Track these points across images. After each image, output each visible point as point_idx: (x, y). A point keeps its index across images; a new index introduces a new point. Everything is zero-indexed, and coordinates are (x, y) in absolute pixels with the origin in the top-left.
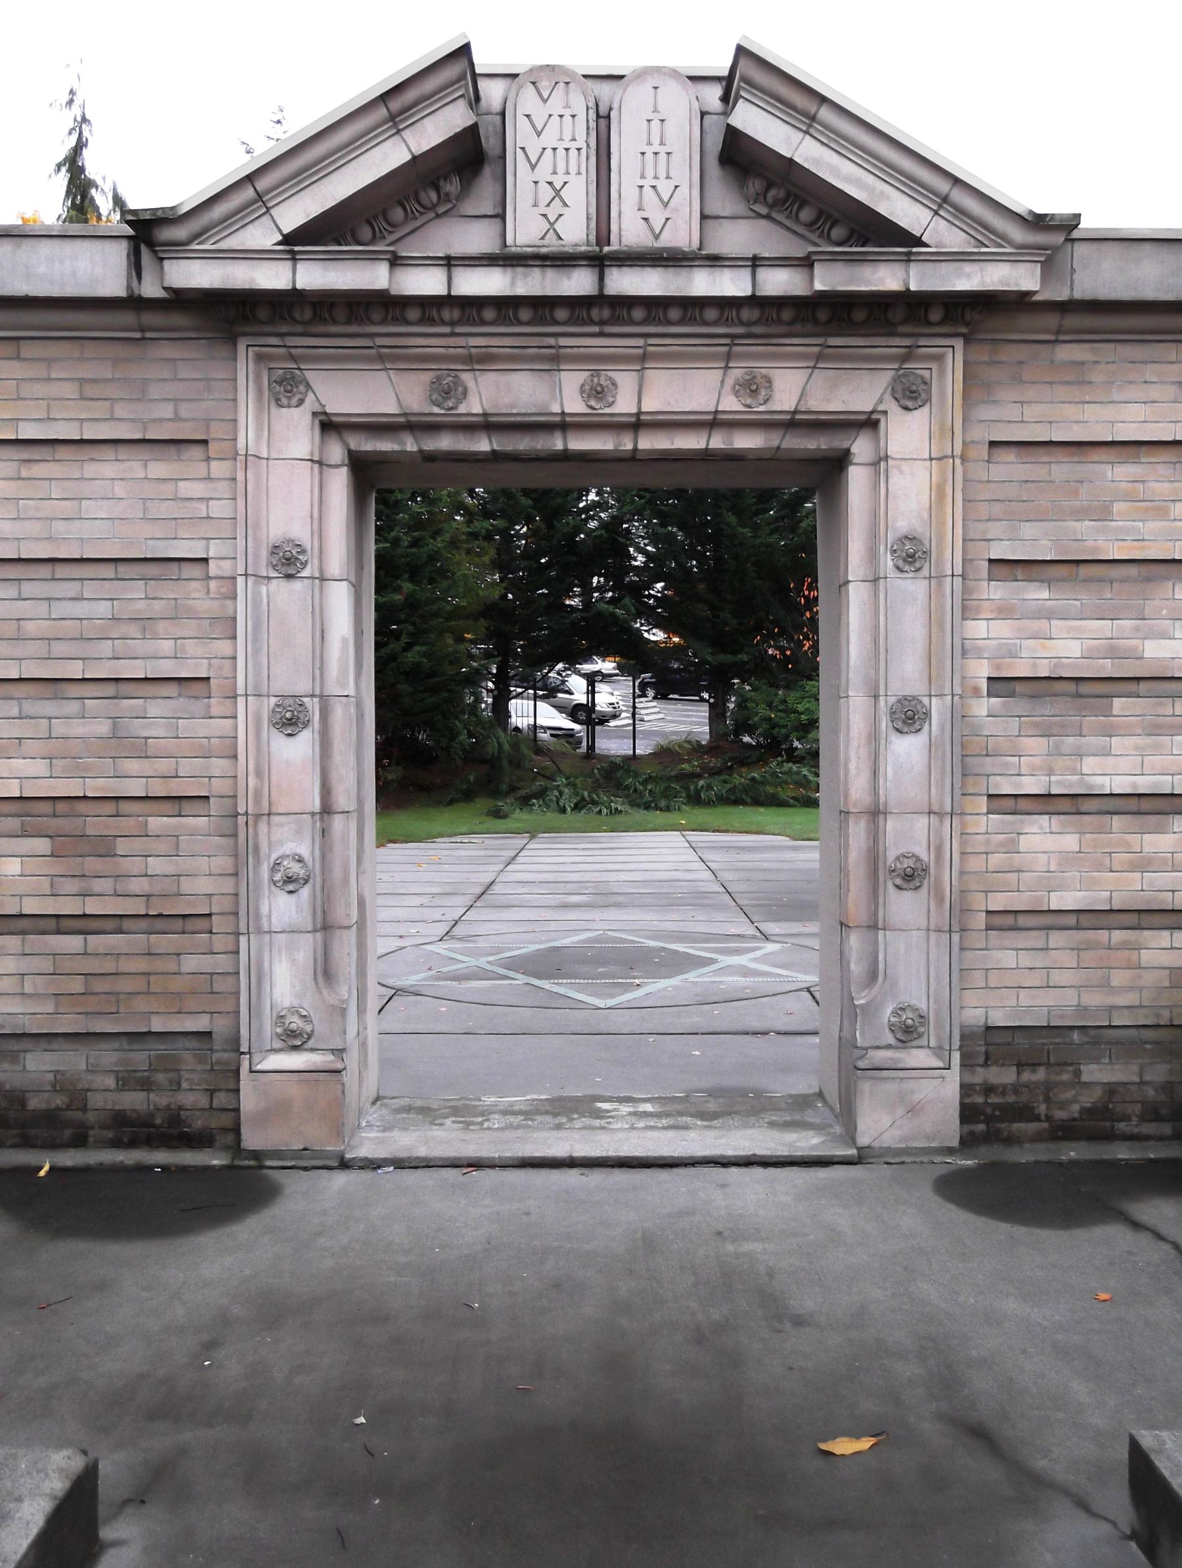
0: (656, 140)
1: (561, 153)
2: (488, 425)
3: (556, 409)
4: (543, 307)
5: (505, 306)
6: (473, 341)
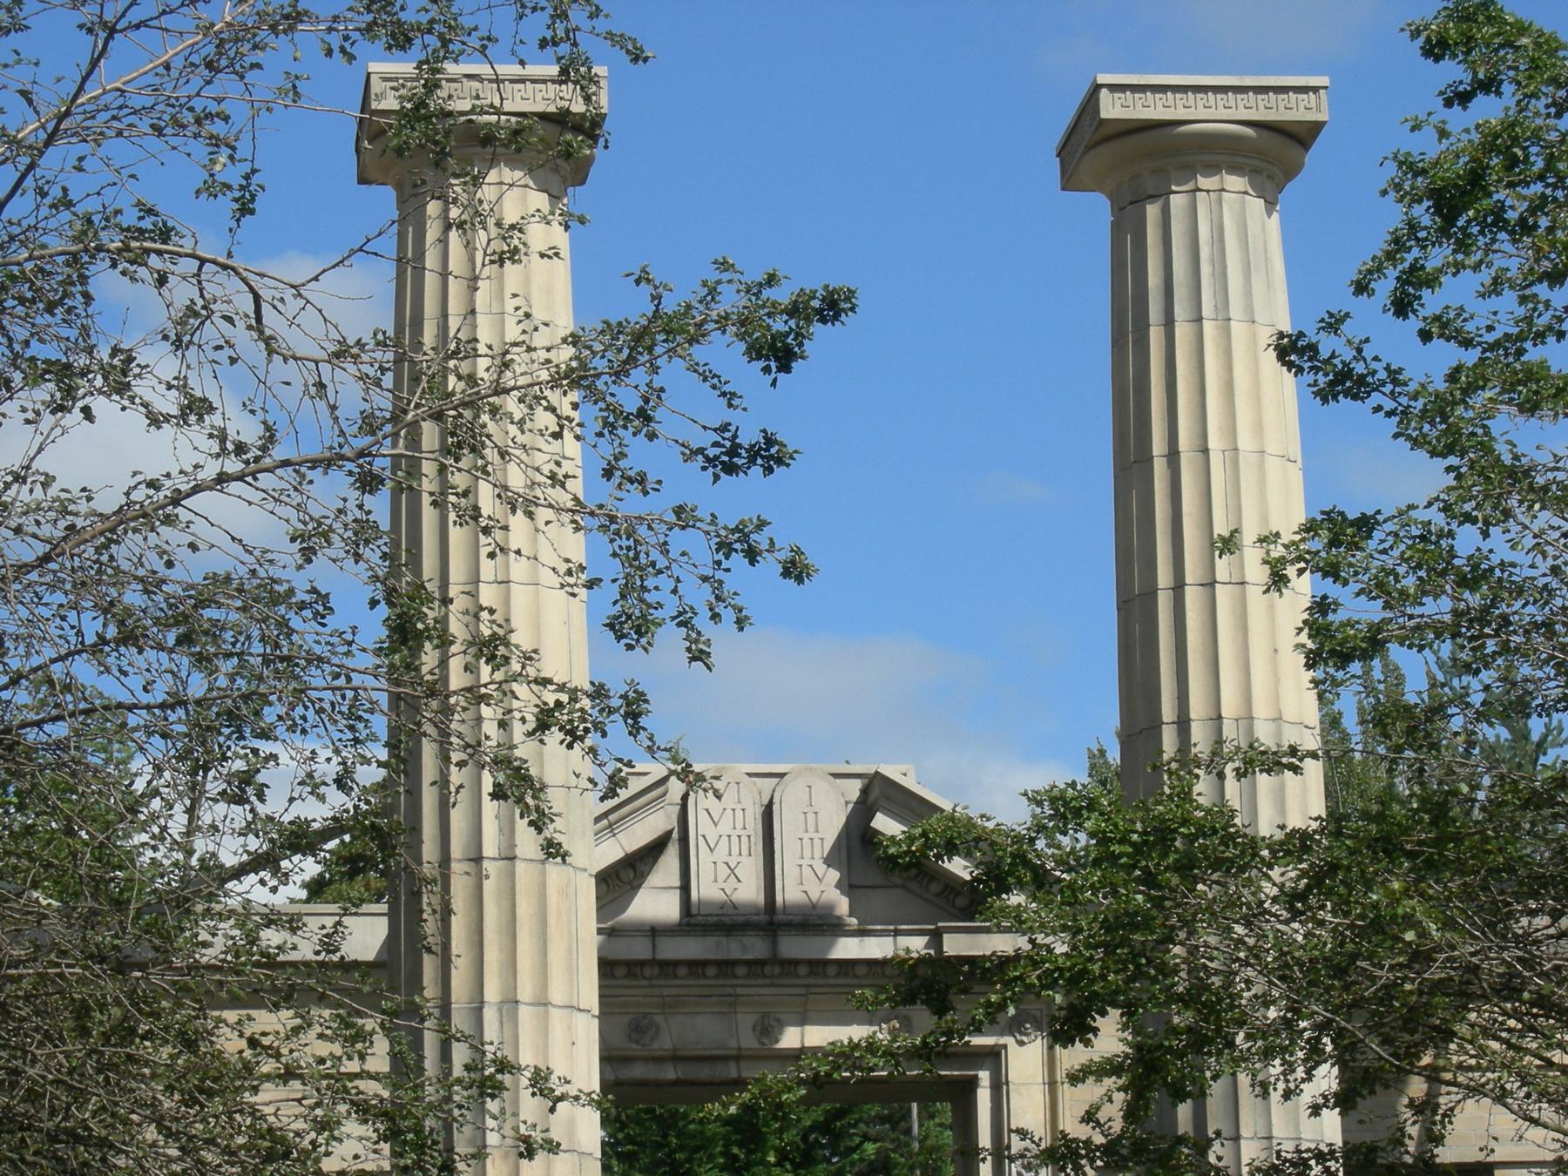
0: (811, 829)
1: (735, 839)
2: (676, 1058)
3: (733, 1044)
4: (726, 966)
5: (696, 966)
6: (666, 991)
